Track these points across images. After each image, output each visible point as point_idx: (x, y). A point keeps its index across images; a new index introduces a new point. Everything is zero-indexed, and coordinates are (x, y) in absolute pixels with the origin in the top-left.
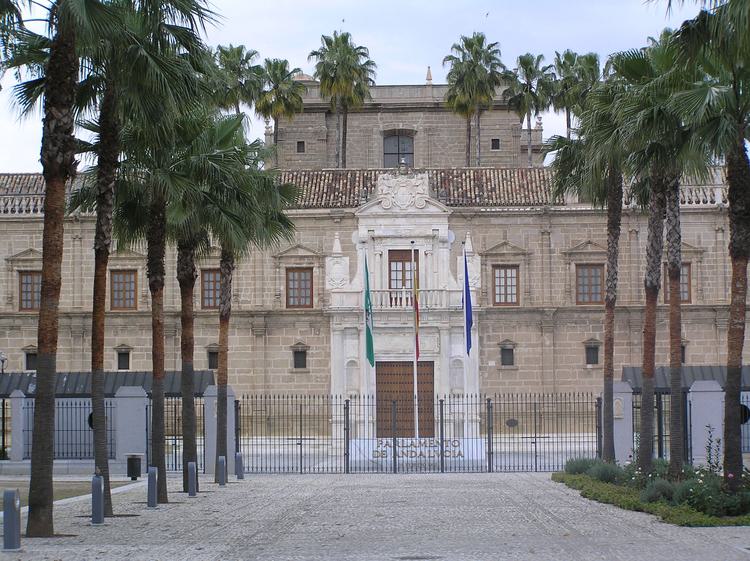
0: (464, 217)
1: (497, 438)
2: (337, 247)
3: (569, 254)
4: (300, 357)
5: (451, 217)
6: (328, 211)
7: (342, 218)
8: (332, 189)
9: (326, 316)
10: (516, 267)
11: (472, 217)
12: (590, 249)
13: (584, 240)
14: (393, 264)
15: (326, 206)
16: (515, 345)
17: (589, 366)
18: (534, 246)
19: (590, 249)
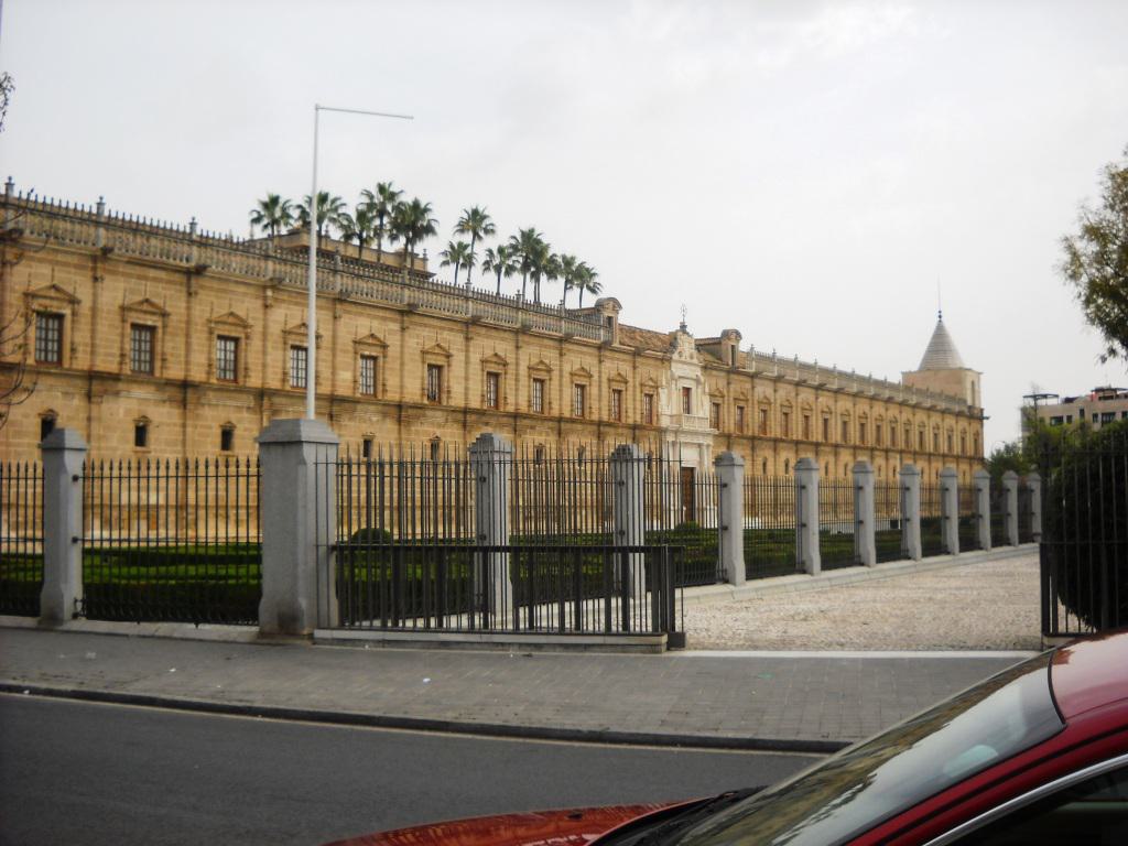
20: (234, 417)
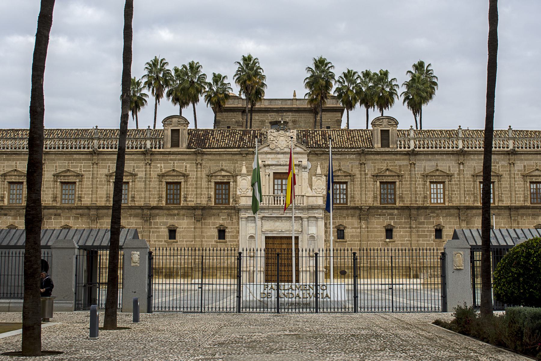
0: (317, 154)
1: (360, 281)
2: (244, 171)
3: (161, 176)
4: (222, 233)
5: (309, 154)
6: (239, 150)
7: (247, 154)
8: (242, 139)
9: (237, 210)
10: (346, 183)
11: (321, 154)
12: (388, 173)
13: (384, 168)
14: (276, 181)
15: (238, 147)
16: (345, 227)
17: (388, 240)
18: (356, 171)
19: (388, 173)
20: (171, 221)
